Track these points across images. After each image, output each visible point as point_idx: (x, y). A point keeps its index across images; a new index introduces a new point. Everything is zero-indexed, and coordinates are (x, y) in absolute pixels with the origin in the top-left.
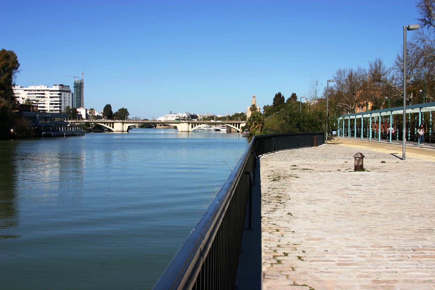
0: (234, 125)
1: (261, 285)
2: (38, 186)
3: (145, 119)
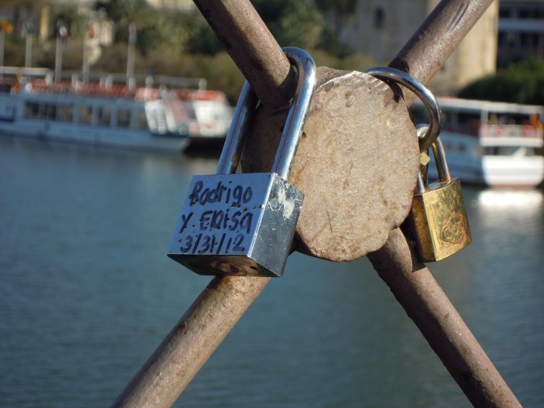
3: (198, 236)
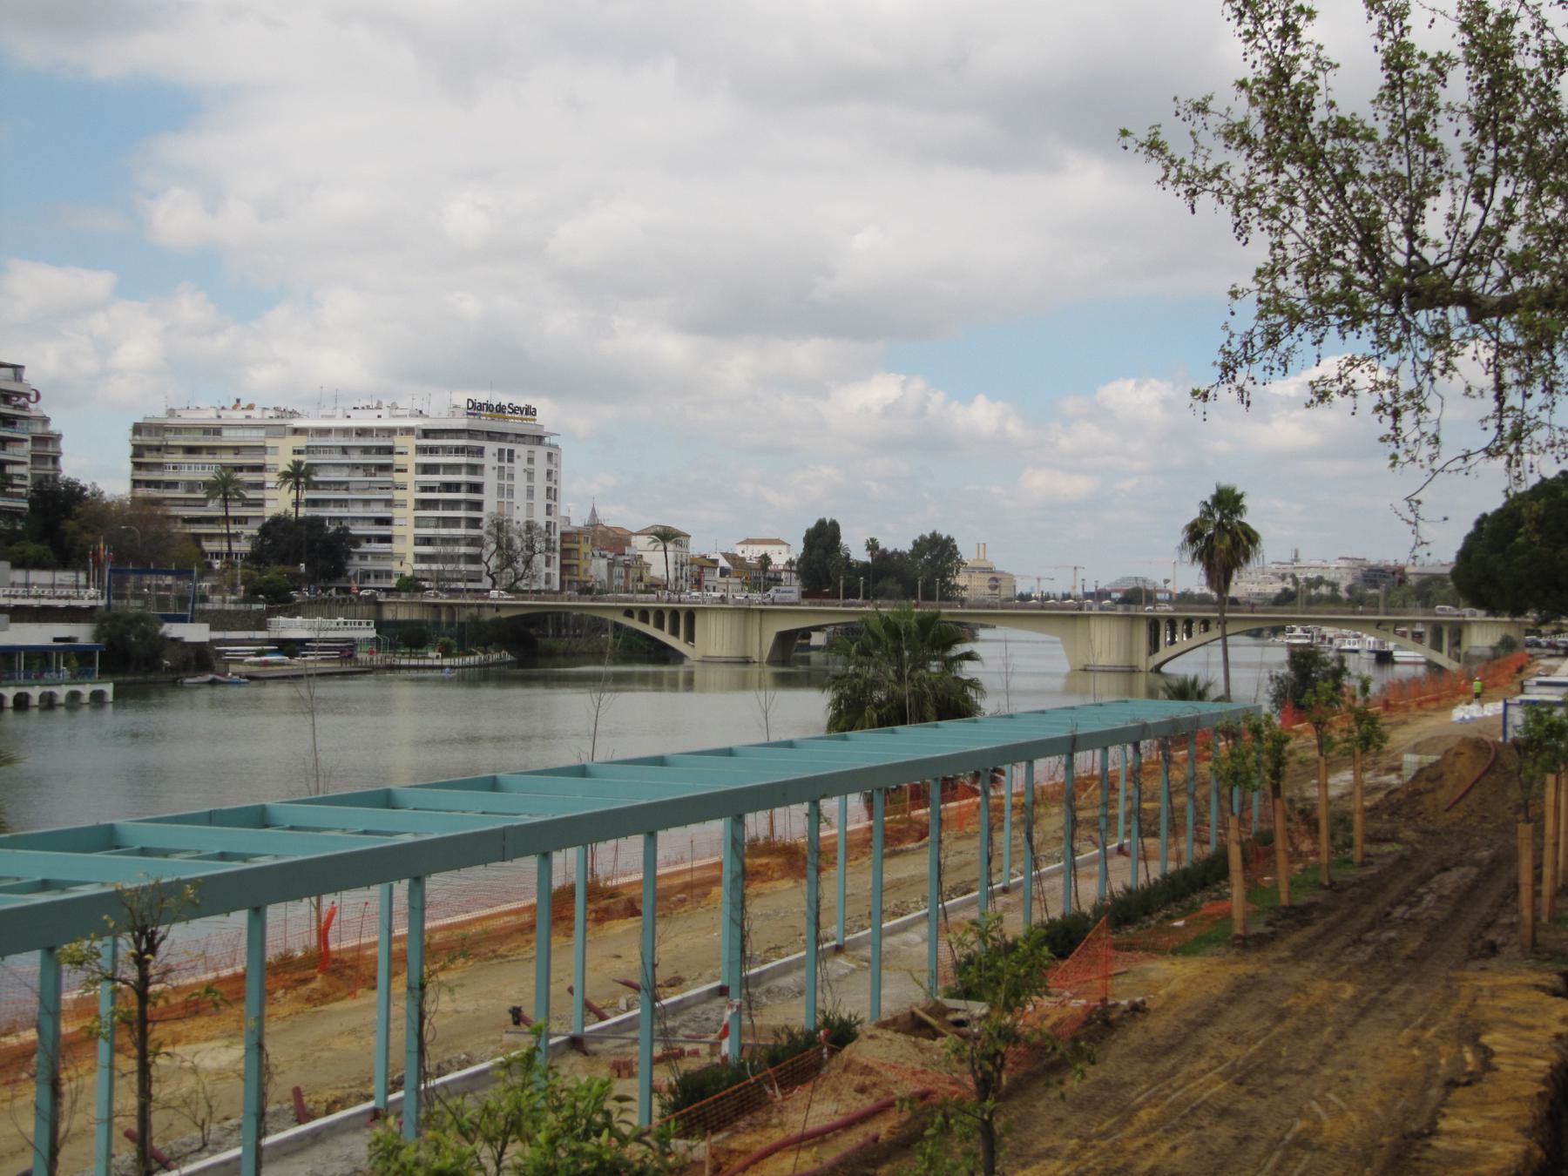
0: (675, 632)
1: (561, 686)
2: (885, 606)
